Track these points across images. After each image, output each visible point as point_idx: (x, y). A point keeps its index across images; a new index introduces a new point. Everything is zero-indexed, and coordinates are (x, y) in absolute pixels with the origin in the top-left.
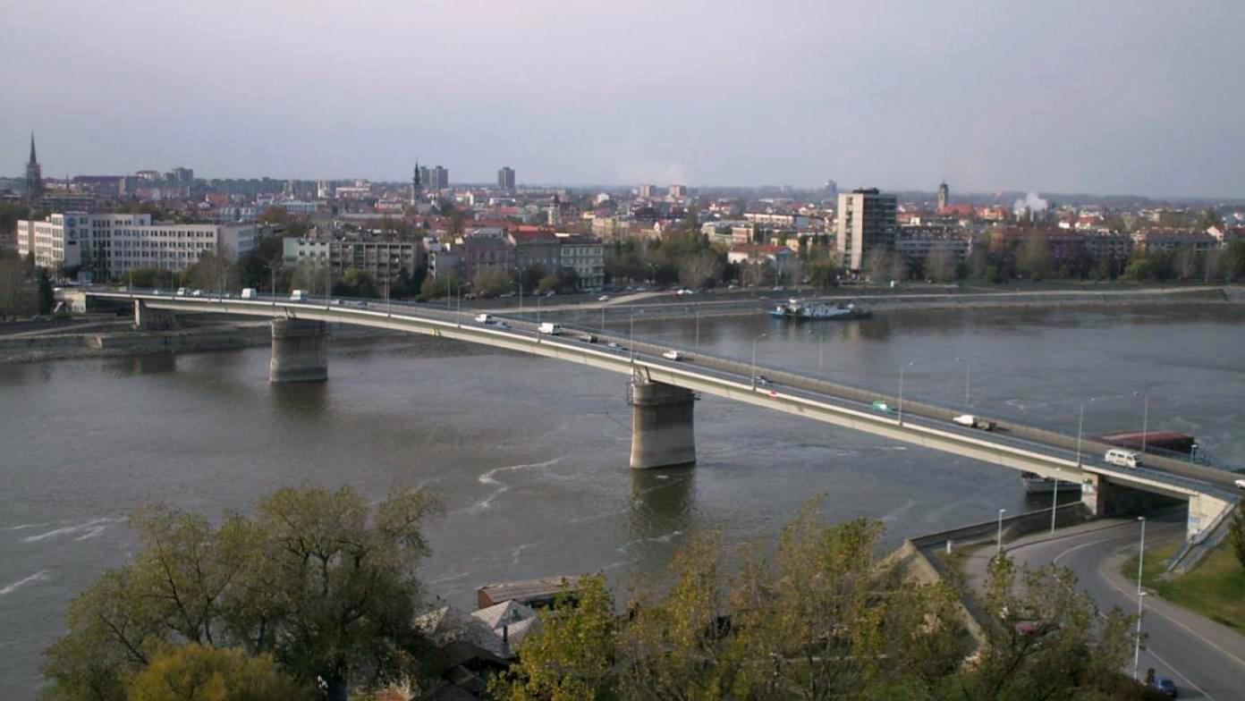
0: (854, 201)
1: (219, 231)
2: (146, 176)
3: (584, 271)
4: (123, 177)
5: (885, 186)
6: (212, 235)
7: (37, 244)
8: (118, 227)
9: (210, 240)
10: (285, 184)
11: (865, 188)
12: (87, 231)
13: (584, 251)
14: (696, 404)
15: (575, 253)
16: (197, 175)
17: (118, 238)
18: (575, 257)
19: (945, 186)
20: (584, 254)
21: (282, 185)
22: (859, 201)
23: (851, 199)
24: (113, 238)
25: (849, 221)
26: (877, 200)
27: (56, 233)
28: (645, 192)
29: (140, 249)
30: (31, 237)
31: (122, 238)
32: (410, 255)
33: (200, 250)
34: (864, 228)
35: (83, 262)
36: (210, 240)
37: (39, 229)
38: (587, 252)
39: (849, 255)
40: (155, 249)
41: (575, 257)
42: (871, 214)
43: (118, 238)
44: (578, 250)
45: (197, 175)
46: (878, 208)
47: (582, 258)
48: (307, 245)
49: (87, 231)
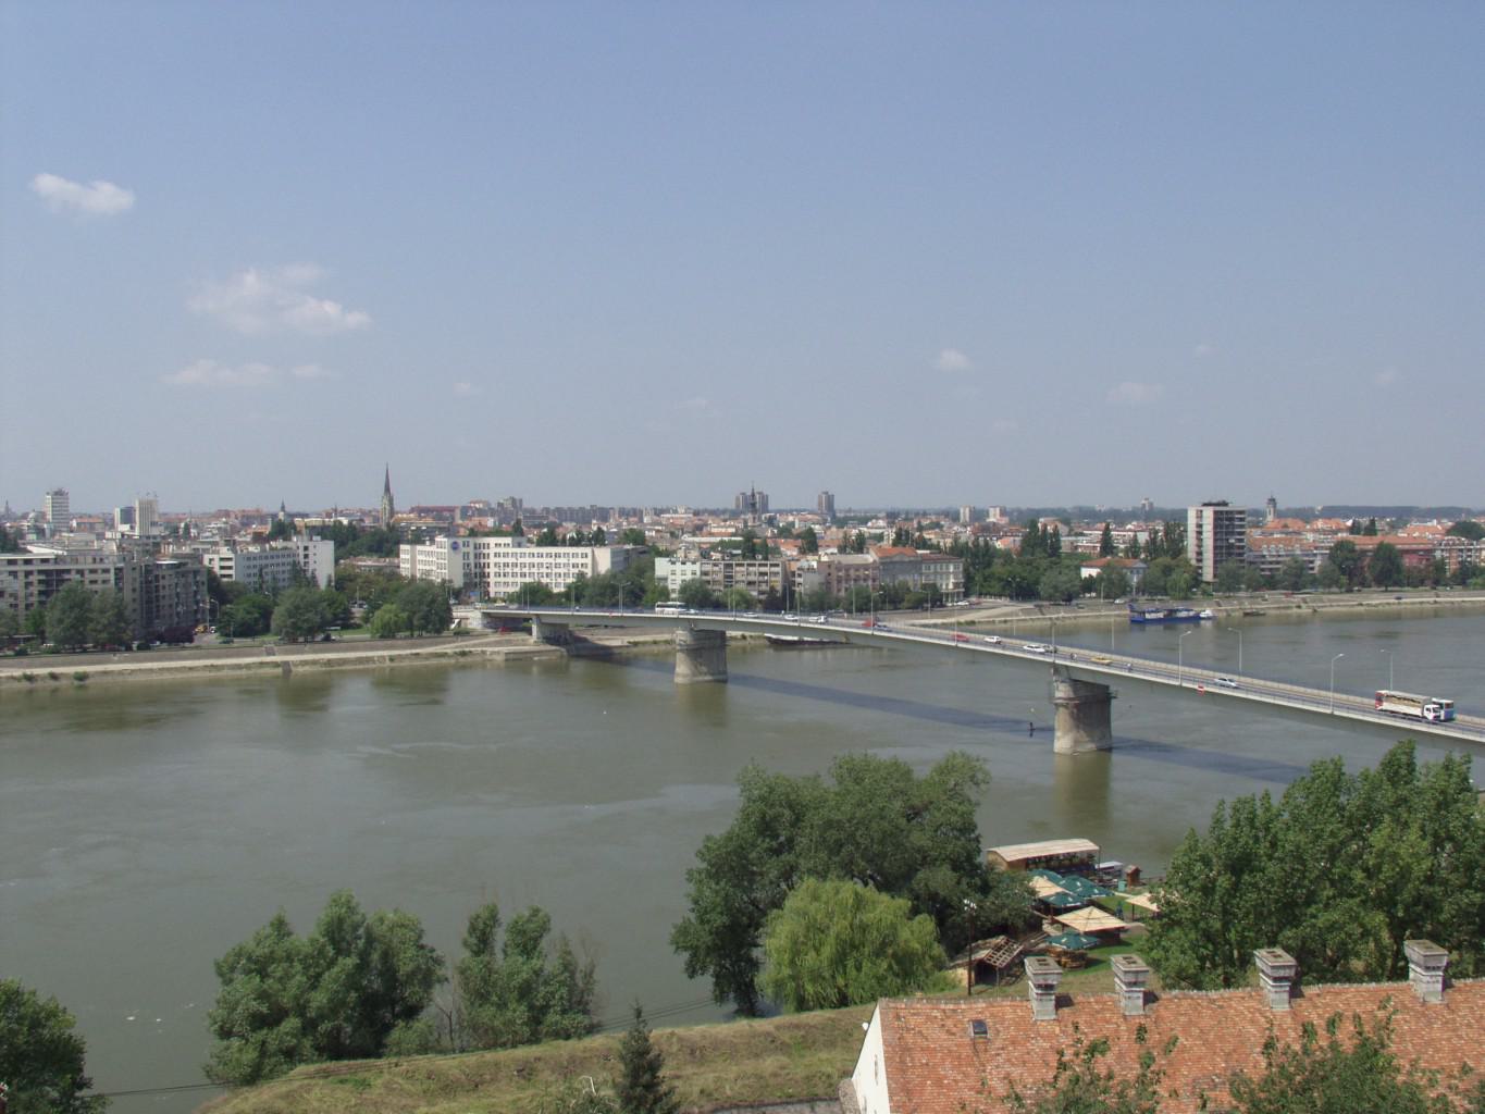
0: (1204, 514)
1: (593, 552)
2: (477, 506)
3: (944, 587)
4: (457, 507)
5: (1236, 503)
6: (495, 554)
7: (420, 567)
8: (498, 550)
9: (584, 561)
10: (611, 511)
11: (1214, 501)
12: (468, 553)
13: (944, 567)
14: (1114, 702)
15: (935, 568)
16: (526, 505)
17: (497, 560)
18: (936, 573)
19: (1272, 501)
20: (944, 570)
21: (608, 512)
22: (1209, 513)
23: (1201, 511)
24: (492, 560)
25: (1200, 533)
26: (1227, 512)
27: (439, 556)
28: (965, 516)
29: (517, 570)
30: (413, 561)
31: (502, 560)
32: (778, 573)
33: (576, 571)
34: (1215, 540)
35: (465, 584)
36: (584, 561)
37: (421, 552)
39: (1201, 568)
40: (533, 570)
41: (936, 573)
42: (1221, 527)
43: (497, 560)
44: (938, 566)
45: (526, 505)
46: (1227, 522)
47: (942, 574)
48: (678, 564)
49: (468, 553)
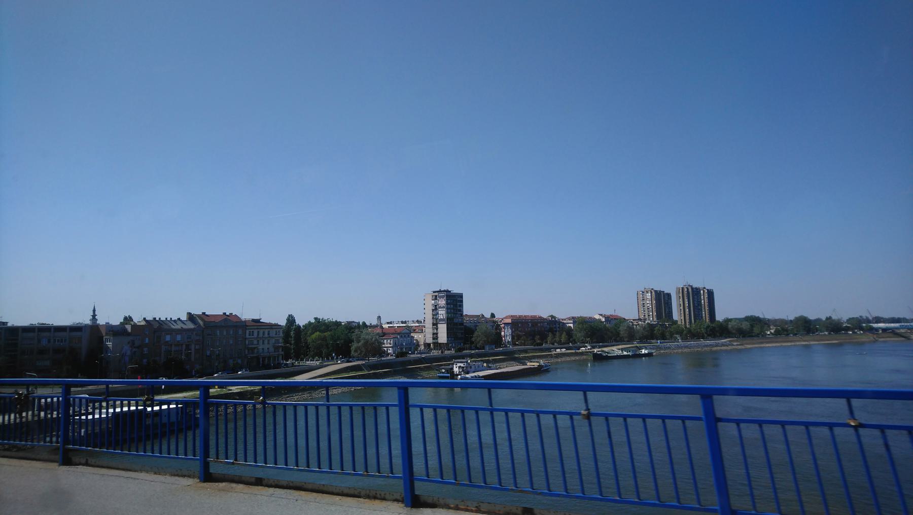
38: (269, 334)
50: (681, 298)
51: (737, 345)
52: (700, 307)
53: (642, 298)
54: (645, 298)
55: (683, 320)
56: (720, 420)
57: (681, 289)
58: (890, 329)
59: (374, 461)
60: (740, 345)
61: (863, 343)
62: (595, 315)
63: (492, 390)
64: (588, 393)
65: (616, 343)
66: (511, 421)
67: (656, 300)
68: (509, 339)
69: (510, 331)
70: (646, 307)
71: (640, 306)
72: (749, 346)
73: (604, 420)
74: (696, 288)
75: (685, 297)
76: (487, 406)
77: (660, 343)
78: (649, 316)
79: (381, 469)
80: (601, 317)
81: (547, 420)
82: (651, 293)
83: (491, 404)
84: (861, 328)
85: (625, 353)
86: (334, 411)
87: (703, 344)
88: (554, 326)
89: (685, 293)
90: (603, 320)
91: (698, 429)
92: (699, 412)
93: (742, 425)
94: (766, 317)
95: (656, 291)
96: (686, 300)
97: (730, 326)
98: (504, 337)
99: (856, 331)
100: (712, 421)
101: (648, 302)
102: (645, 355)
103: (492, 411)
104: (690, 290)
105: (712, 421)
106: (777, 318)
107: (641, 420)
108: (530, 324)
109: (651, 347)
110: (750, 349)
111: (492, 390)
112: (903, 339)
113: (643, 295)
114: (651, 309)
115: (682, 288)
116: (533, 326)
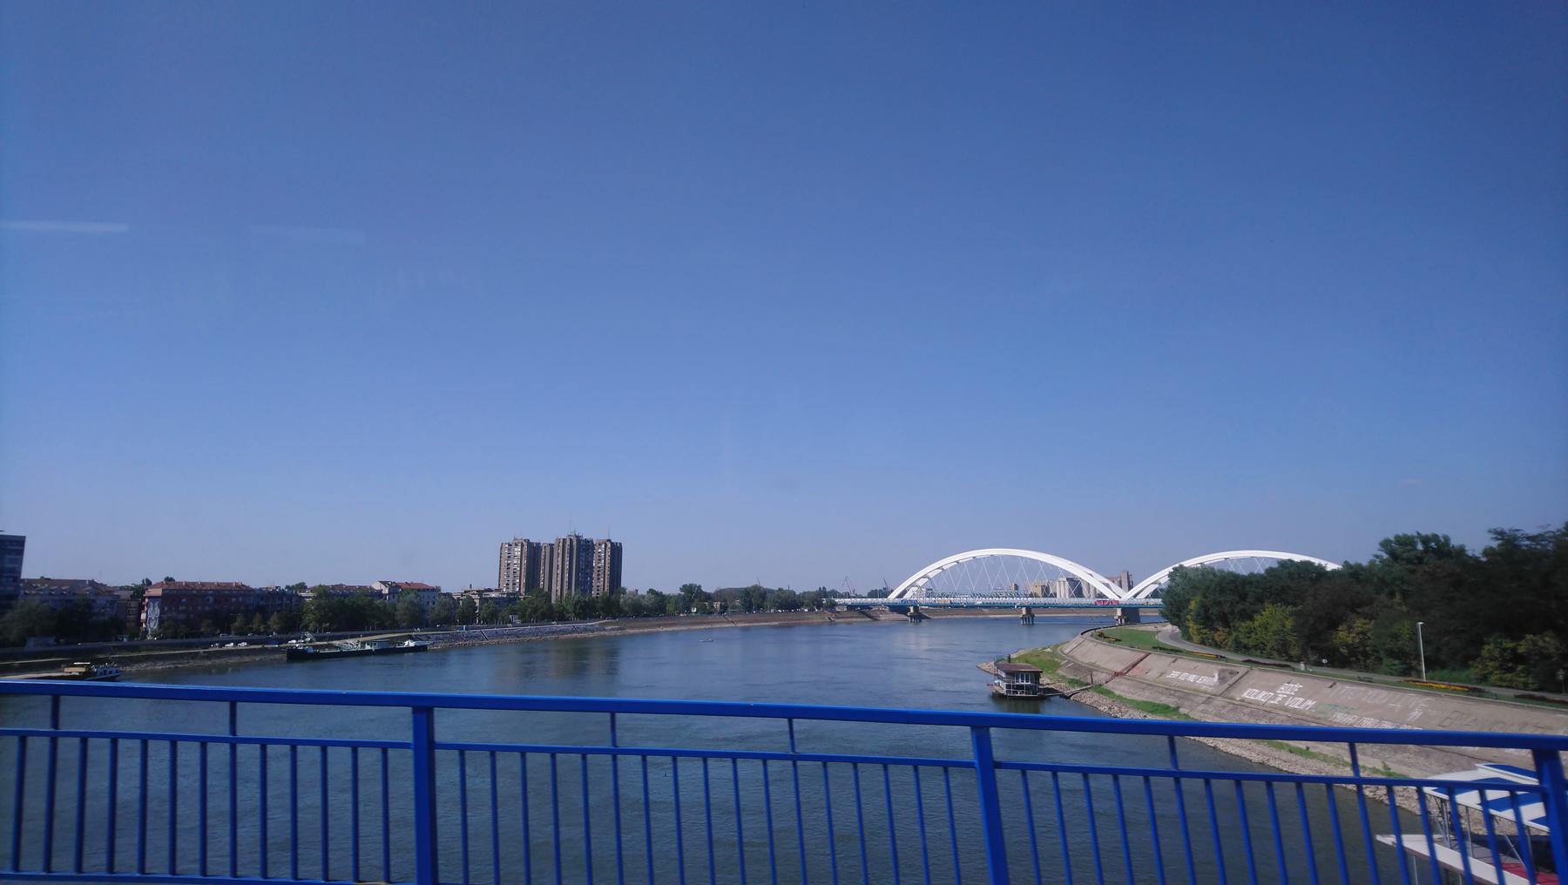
50: (561, 556)
51: (612, 629)
52: (588, 571)
53: (507, 555)
54: (512, 555)
55: (559, 590)
56: (999, 765)
57: (562, 541)
58: (857, 606)
59: (40, 825)
60: (618, 629)
61: (820, 625)
62: (374, 582)
63: (239, 705)
64: (794, 720)
65: (381, 631)
66: (181, 758)
67: (529, 558)
68: (153, 626)
69: (158, 611)
70: (511, 571)
71: (502, 567)
72: (632, 631)
73: (1234, 787)
74: (586, 541)
75: (567, 555)
76: (1166, 765)
77: (466, 629)
78: (514, 584)
79: (362, 870)
80: (383, 587)
81: (1256, 791)
82: (522, 546)
83: (233, 730)
84: (820, 606)
85: (368, 647)
86: (69, 750)
87: (548, 630)
88: (279, 602)
89: (567, 547)
90: (386, 591)
91: (402, 763)
92: (970, 755)
93: (892, 768)
94: (762, 585)
95: (530, 544)
96: (567, 559)
97: (622, 600)
98: (146, 623)
99: (209, 630)
100: (425, 747)
101: (515, 562)
102: (409, 649)
103: (233, 743)
104: (575, 543)
105: (425, 747)
106: (723, 588)
107: (880, 766)
108: (211, 599)
109: (441, 636)
110: (633, 635)
111: (239, 705)
112: (869, 619)
113: (509, 550)
114: (518, 573)
115: (564, 540)
116: (216, 601)
